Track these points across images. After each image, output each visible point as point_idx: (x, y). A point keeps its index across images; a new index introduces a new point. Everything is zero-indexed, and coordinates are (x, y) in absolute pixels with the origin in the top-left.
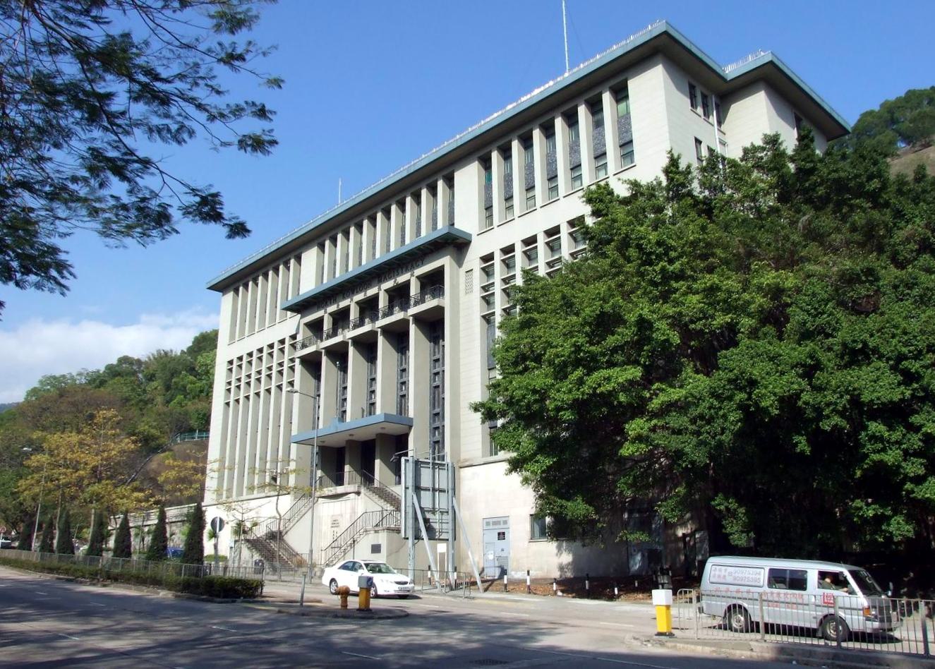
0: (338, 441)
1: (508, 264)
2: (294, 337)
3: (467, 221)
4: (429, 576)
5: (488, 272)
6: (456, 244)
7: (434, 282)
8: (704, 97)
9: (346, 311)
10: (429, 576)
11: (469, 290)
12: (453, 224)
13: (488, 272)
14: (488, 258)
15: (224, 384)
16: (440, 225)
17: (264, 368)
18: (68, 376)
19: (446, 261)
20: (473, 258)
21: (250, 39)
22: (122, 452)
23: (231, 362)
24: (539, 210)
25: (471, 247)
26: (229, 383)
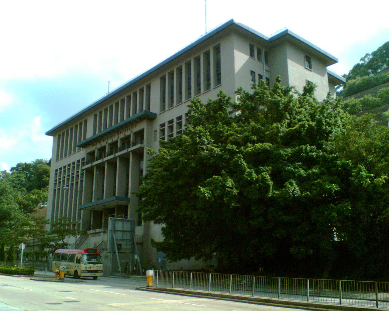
0: (100, 208)
1: (171, 128)
2: (83, 159)
3: (155, 108)
4: (143, 270)
5: (163, 131)
6: (150, 118)
7: (140, 135)
8: (259, 53)
9: (104, 148)
10: (143, 270)
11: (155, 140)
12: (149, 109)
13: (163, 131)
14: (163, 125)
15: (54, 181)
16: (144, 109)
17: (62, 177)
18: (314, 84)
19: (143, 125)
20: (157, 127)
21: (217, 95)
22: (249, 101)
23: (56, 170)
24: (184, 104)
25: (178, 116)
26: (56, 180)
